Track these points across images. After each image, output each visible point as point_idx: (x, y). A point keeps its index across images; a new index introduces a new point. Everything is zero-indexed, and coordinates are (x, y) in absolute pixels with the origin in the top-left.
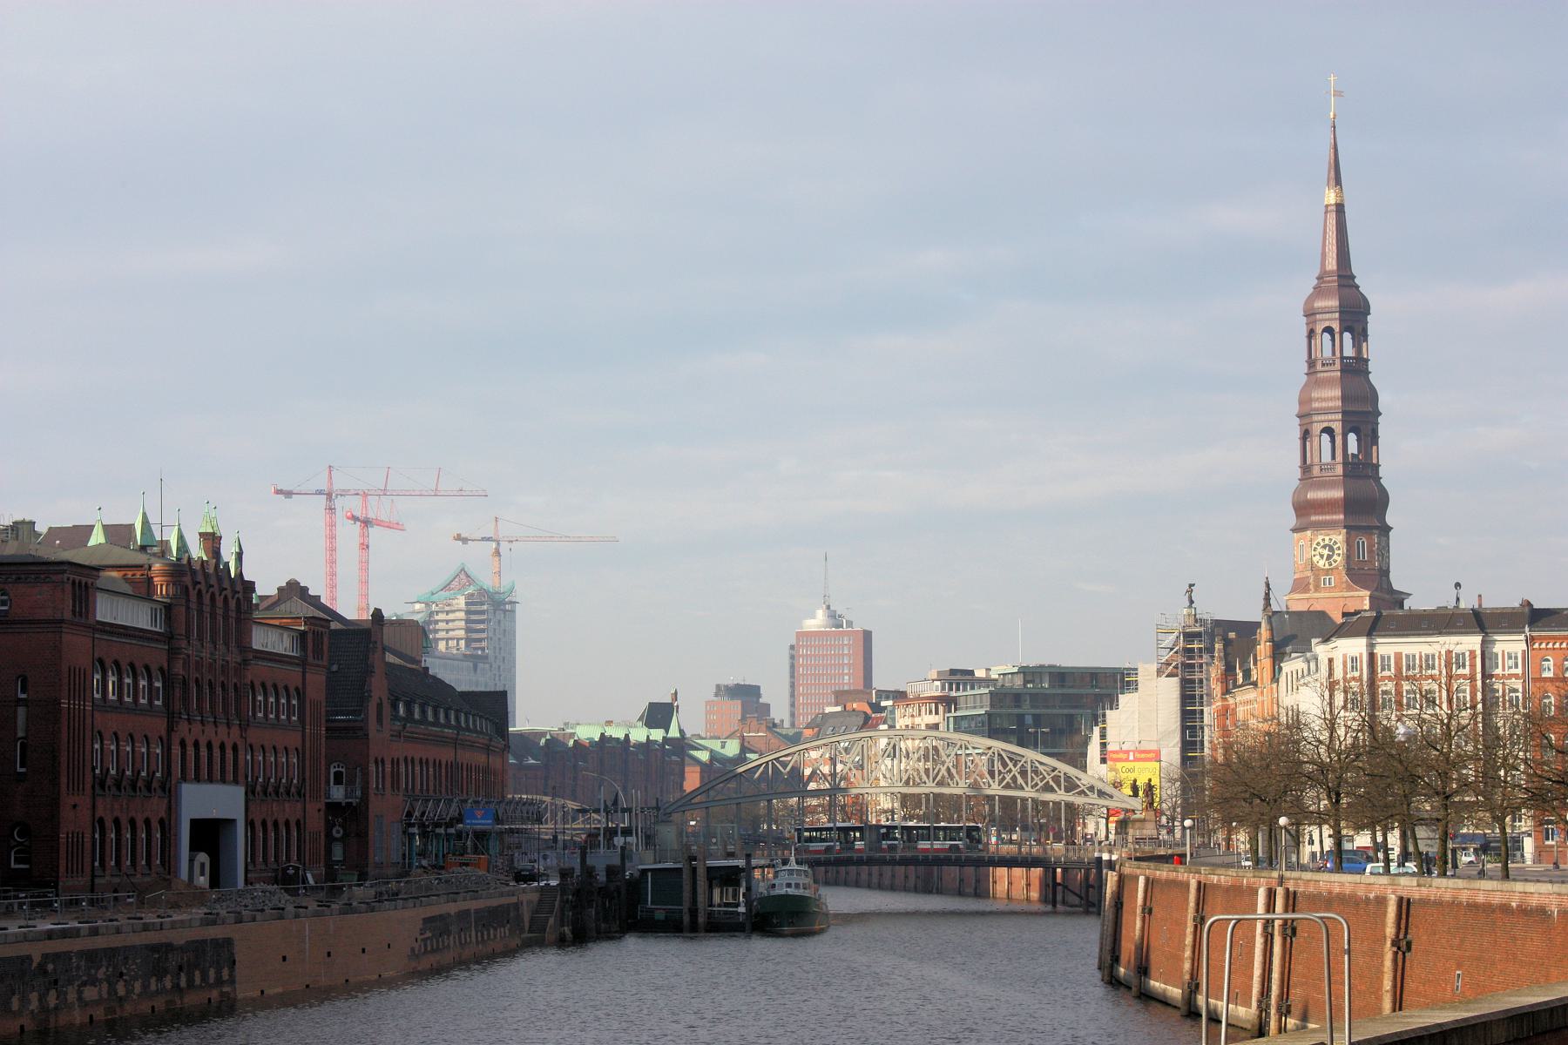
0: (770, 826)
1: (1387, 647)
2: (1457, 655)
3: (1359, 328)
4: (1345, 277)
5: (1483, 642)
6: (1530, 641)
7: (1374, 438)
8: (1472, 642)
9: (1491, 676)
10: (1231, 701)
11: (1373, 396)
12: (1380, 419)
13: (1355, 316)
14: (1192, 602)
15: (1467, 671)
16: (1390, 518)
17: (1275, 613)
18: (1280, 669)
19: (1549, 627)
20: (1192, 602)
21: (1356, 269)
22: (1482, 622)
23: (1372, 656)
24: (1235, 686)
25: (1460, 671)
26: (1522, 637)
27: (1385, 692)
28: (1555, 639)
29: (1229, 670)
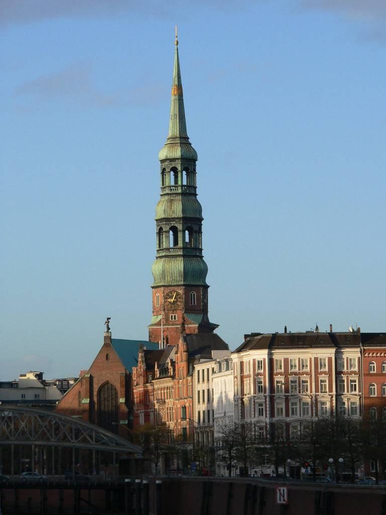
0: (336, 461)
1: (280, 355)
2: (302, 359)
3: (191, 169)
4: (183, 140)
5: (336, 353)
6: (363, 352)
7: (199, 232)
8: (330, 352)
9: (342, 372)
10: (150, 388)
11: (199, 209)
12: (203, 222)
13: (189, 162)
14: (109, 329)
15: (327, 369)
16: (208, 281)
17: (187, 335)
18: (194, 368)
19: (370, 344)
20: (109, 329)
21: (189, 134)
22: (336, 340)
23: (271, 361)
24: (153, 379)
25: (323, 370)
26: (358, 350)
27: (278, 382)
28: (377, 351)
29: (149, 368)
